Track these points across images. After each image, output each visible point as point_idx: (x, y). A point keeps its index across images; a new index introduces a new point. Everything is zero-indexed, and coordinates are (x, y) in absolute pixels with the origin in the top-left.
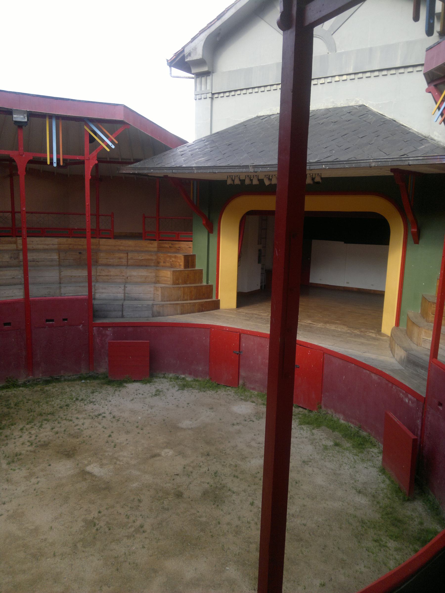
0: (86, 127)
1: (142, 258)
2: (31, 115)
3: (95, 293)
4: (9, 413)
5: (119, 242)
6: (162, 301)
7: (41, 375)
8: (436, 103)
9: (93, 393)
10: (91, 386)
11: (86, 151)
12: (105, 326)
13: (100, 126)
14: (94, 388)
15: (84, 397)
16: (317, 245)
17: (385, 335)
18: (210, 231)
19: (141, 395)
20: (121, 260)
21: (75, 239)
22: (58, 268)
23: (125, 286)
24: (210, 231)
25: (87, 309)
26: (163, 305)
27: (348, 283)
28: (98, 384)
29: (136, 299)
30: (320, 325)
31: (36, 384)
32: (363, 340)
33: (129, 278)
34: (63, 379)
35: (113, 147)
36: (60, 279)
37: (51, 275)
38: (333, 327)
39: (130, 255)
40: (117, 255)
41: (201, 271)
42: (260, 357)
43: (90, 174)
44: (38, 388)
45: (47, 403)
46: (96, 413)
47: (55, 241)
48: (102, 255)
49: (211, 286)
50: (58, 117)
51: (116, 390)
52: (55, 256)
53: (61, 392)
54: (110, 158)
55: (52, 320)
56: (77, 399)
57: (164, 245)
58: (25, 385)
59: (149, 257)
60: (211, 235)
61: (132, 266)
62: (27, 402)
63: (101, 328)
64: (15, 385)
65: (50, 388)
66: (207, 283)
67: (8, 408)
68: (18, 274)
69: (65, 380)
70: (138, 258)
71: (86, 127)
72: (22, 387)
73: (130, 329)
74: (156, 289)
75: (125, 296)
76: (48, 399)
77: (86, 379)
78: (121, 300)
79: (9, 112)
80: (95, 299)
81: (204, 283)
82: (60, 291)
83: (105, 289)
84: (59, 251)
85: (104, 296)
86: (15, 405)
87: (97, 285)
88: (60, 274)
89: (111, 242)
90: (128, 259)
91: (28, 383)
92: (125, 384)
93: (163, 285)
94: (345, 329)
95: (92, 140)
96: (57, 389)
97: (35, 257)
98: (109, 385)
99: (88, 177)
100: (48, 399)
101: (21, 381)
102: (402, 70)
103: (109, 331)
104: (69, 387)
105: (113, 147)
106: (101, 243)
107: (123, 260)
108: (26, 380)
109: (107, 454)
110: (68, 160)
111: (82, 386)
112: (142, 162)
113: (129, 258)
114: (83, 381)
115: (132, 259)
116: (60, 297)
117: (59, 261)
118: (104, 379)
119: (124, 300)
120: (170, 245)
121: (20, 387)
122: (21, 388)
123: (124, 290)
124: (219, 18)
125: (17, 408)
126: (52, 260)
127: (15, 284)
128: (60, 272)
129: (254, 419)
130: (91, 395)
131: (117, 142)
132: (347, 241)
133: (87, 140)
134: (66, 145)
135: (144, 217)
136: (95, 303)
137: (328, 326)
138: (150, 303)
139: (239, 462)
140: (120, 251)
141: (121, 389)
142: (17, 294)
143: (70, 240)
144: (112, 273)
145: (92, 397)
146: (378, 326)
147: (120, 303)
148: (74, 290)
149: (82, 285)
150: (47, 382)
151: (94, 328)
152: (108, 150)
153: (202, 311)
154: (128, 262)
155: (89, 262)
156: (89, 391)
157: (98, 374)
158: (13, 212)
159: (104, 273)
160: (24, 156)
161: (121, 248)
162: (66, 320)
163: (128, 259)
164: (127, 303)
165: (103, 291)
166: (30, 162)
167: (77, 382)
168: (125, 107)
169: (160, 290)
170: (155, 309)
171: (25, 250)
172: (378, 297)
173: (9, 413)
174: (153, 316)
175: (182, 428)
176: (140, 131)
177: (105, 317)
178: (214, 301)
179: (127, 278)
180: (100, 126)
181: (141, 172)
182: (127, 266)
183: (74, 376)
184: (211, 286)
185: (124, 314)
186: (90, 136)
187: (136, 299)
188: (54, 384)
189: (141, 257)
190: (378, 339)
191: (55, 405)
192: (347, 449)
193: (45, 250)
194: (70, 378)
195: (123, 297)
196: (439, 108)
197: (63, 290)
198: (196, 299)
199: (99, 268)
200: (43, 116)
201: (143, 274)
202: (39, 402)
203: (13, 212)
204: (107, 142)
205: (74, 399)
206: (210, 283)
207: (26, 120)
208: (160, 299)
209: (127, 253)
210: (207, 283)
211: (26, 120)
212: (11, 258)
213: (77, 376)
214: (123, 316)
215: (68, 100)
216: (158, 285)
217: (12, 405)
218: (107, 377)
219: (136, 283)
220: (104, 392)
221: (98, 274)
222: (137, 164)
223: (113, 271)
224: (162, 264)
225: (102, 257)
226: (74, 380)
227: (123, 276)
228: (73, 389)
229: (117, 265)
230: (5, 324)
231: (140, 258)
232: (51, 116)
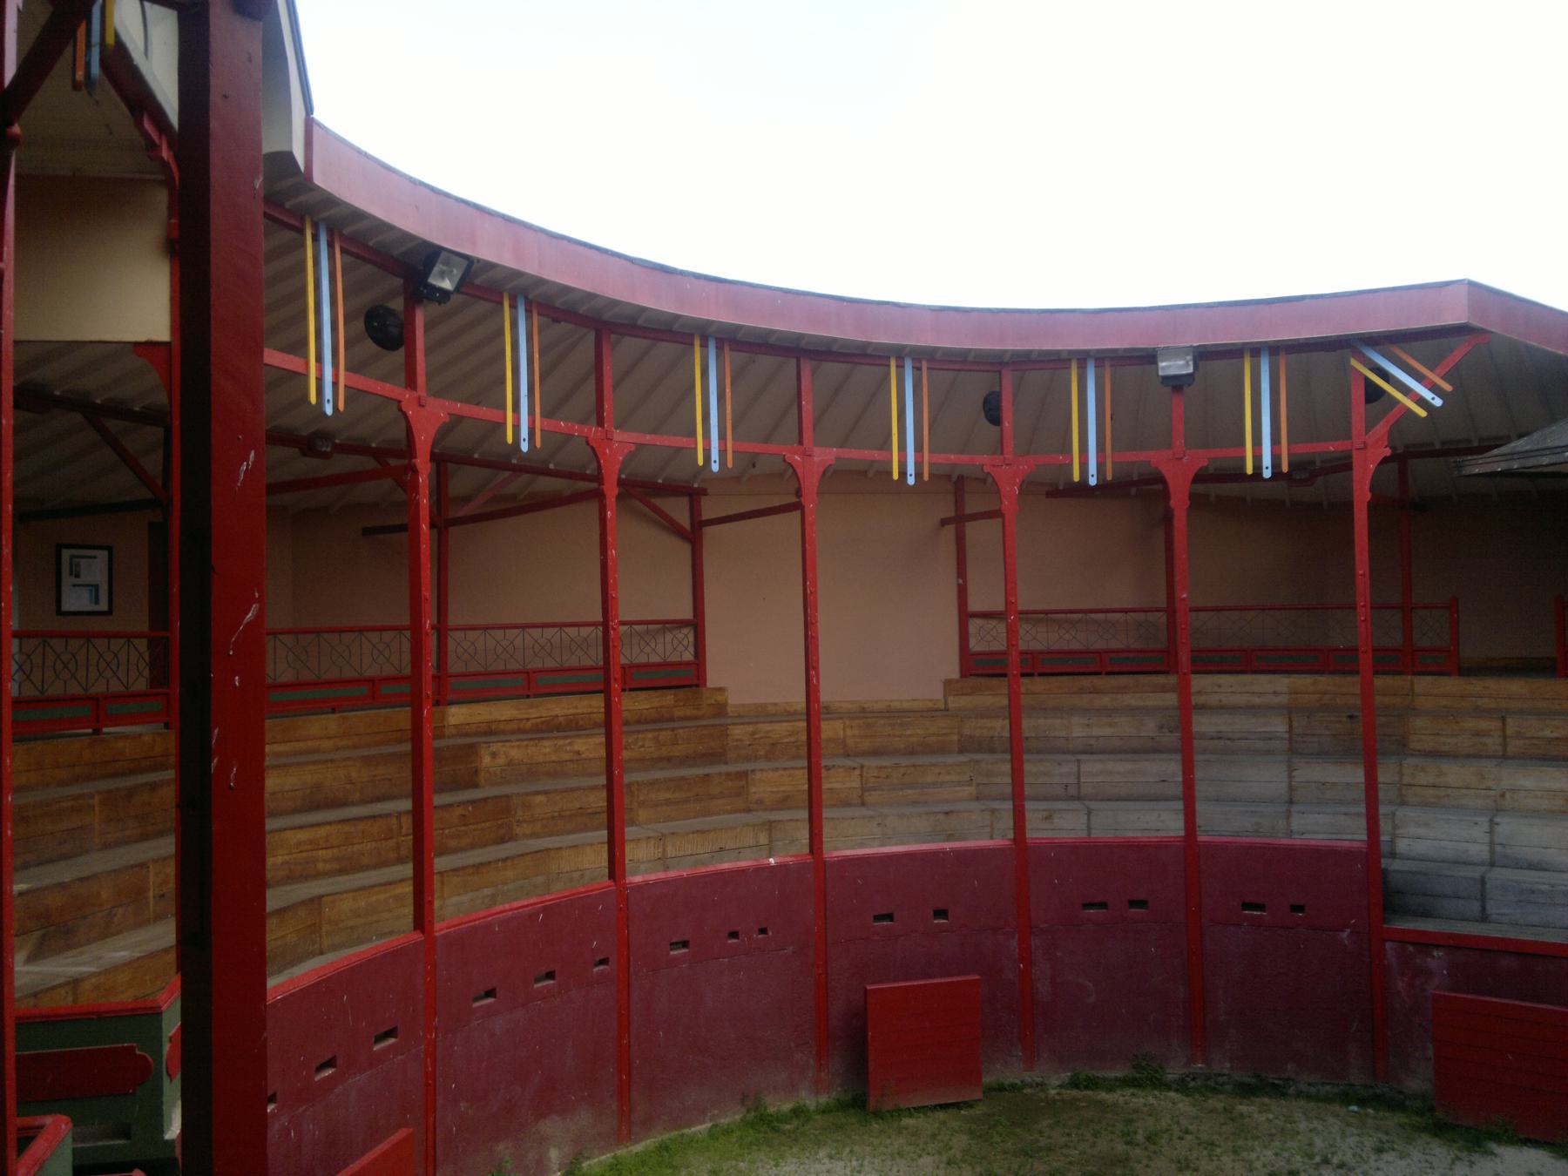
0: (1354, 363)
1: (1555, 735)
2: (1203, 355)
3: (1394, 837)
4: (1128, 1159)
5: (1477, 685)
7: (1228, 1065)
9: (1379, 1151)
10: (1377, 1129)
12: (1425, 943)
13: (1399, 352)
14: (1385, 1138)
15: (1348, 1158)
20: (1484, 740)
21: (1337, 679)
23: (1491, 820)
25: (1365, 884)
28: (1402, 1126)
29: (1531, 866)
31: (1215, 1091)
33: (1508, 796)
34: (1292, 1090)
36: (1291, 789)
37: (1267, 778)
39: (1512, 725)
40: (1470, 724)
43: (1367, 487)
44: (1216, 1103)
45: (1235, 1152)
47: (1283, 683)
48: (1419, 722)
50: (1275, 349)
51: (1458, 1158)
52: (1279, 726)
53: (1283, 1130)
54: (1443, 443)
55: (1261, 907)
56: (1326, 1161)
58: (1182, 1086)
62: (1181, 1138)
63: (1411, 948)
64: (1158, 1084)
65: (1252, 1108)
67: (1127, 1143)
68: (1171, 767)
69: (1299, 1095)
70: (1541, 734)
71: (1354, 363)
72: (1177, 1091)
75: (1492, 851)
76: (1240, 1142)
77: (1362, 1102)
78: (1482, 864)
79: (1149, 358)
80: (1393, 855)
82: (1289, 824)
83: (1426, 825)
84: (1290, 711)
85: (1420, 848)
86: (1148, 1139)
87: (1401, 813)
88: (1290, 777)
89: (1452, 684)
90: (1505, 737)
91: (1192, 1084)
92: (1493, 1146)
95: (1373, 394)
96: (1271, 1116)
97: (1223, 728)
98: (1436, 1135)
99: (1362, 495)
100: (1240, 1142)
101: (1173, 1073)
103: (1437, 960)
104: (1309, 1119)
106: (1418, 688)
107: (1489, 741)
108: (1186, 1071)
110: (1318, 464)
111: (1348, 1124)
112: (1535, 436)
113: (1509, 732)
114: (1355, 1108)
116: (1285, 841)
117: (1290, 739)
118: (1420, 1113)
119: (1492, 864)
121: (1169, 1089)
122: (1172, 1094)
123: (1491, 832)
125: (1152, 1148)
126: (1269, 737)
127: (1167, 799)
128: (1291, 770)
130: (1373, 1157)
131: (1448, 387)
133: (1359, 393)
134: (1302, 418)
136: (1392, 868)
140: (1479, 712)
141: (1475, 1157)
142: (1166, 823)
145: (1374, 1164)
147: (1476, 873)
148: (1328, 824)
149: (1353, 809)
150: (1246, 1091)
151: (1388, 945)
154: (1504, 745)
155: (1371, 743)
156: (1369, 1143)
157: (1401, 1092)
158: (1171, 611)
159: (1422, 779)
160: (1185, 460)
162: (1300, 908)
163: (1505, 737)
164: (1499, 875)
165: (1421, 831)
166: (1200, 478)
167: (1337, 1107)
168: (1473, 286)
171: (1186, 709)
173: (1128, 1159)
176: (1527, 346)
177: (1427, 914)
179: (1503, 796)
180: (1399, 352)
182: (1504, 757)
183: (1328, 1088)
185: (1492, 909)
187: (1531, 866)
188: (1266, 1100)
191: (1258, 1165)
193: (1251, 710)
194: (1313, 1090)
195: (1486, 856)
197: (1297, 823)
199: (1410, 762)
200: (1234, 353)
201: (1557, 785)
202: (1213, 1144)
204: (1417, 392)
205: (1318, 1159)
209: (1503, 719)
213: (1336, 1090)
214: (1484, 918)
215: (1303, 298)
217: (1140, 1137)
218: (1432, 1109)
219: (1533, 813)
220: (1417, 1155)
221: (1406, 780)
222: (1521, 441)
223: (1454, 773)
226: (1327, 1100)
227: (1489, 789)
228: (1320, 1127)
230: (1133, 903)
231: (1547, 733)
232: (1255, 350)
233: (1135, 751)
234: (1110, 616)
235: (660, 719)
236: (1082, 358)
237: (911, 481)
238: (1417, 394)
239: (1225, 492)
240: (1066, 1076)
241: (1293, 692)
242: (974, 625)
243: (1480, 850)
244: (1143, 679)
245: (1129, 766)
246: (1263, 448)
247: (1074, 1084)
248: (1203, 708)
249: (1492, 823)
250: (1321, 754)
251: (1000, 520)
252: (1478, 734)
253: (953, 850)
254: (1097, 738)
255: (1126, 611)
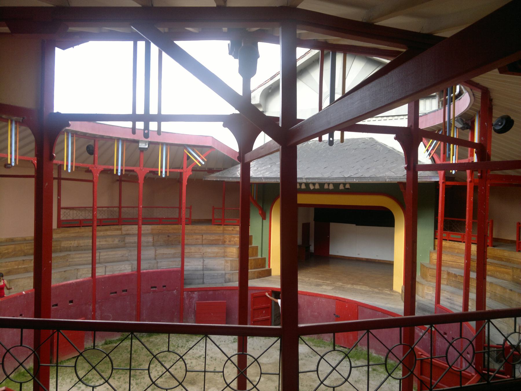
6: (231, 270)
8: (426, 147)
11: (185, 166)
12: (193, 291)
16: (334, 227)
17: (396, 292)
18: (264, 218)
19: (223, 342)
22: (153, 248)
24: (264, 218)
26: (233, 274)
27: (359, 254)
29: (211, 270)
30: (349, 286)
32: (382, 296)
35: (203, 163)
38: (359, 287)
40: (195, 237)
41: (257, 247)
42: (309, 311)
46: (198, 355)
49: (265, 259)
50: (167, 144)
55: (156, 287)
57: (227, 229)
59: (218, 238)
60: (264, 221)
61: (205, 244)
66: (262, 256)
73: (211, 293)
74: (226, 261)
81: (259, 257)
83: (189, 262)
93: (231, 259)
94: (368, 289)
95: (188, 158)
99: (185, 182)
102: (396, 117)
103: (195, 295)
105: (203, 163)
107: (199, 241)
109: (218, 381)
112: (221, 172)
115: (205, 239)
120: (233, 228)
123: (203, 263)
124: (272, 78)
129: (311, 356)
131: (206, 160)
132: (357, 224)
133: (185, 158)
135: (214, 208)
137: (355, 287)
138: (223, 272)
139: (312, 383)
140: (195, 233)
143: (159, 227)
144: (193, 251)
146: (390, 285)
147: (202, 272)
148: (174, 264)
152: (200, 165)
153: (260, 277)
156: (184, 340)
158: (120, 207)
161: (197, 231)
162: (165, 286)
164: (205, 272)
169: (229, 262)
170: (227, 276)
172: (390, 265)
174: (225, 283)
175: (448, 292)
177: (190, 284)
178: (267, 270)
181: (222, 180)
184: (265, 259)
185: (205, 281)
186: (188, 156)
187: (211, 270)
189: (212, 238)
190: (392, 295)
192: (382, 373)
196: (427, 150)
197: (159, 265)
198: (254, 269)
201: (215, 251)
203: (120, 207)
204: (199, 160)
206: (264, 256)
207: (147, 147)
208: (229, 269)
210: (262, 256)
211: (147, 147)
212: (119, 241)
214: (203, 283)
216: (227, 259)
219: (210, 257)
222: (218, 173)
224: (227, 242)
225: (188, 239)
229: (194, 245)
230: (123, 291)
231: (211, 238)
233: (112, 248)
234: (104, 209)
235: (230, 281)
236: (118, 139)
237: (69, 171)
238: (437, 219)
239: (153, 180)
240: (103, 342)
241: (152, 230)
242: (62, 211)
243: (200, 267)
244: (112, 227)
245: (114, 253)
246: (163, 170)
247: (106, 344)
248: (188, 245)
249: (204, 261)
250: (161, 246)
251: (92, 183)
252: (197, 239)
253: (75, 282)
254: (102, 245)
255: (108, 207)
